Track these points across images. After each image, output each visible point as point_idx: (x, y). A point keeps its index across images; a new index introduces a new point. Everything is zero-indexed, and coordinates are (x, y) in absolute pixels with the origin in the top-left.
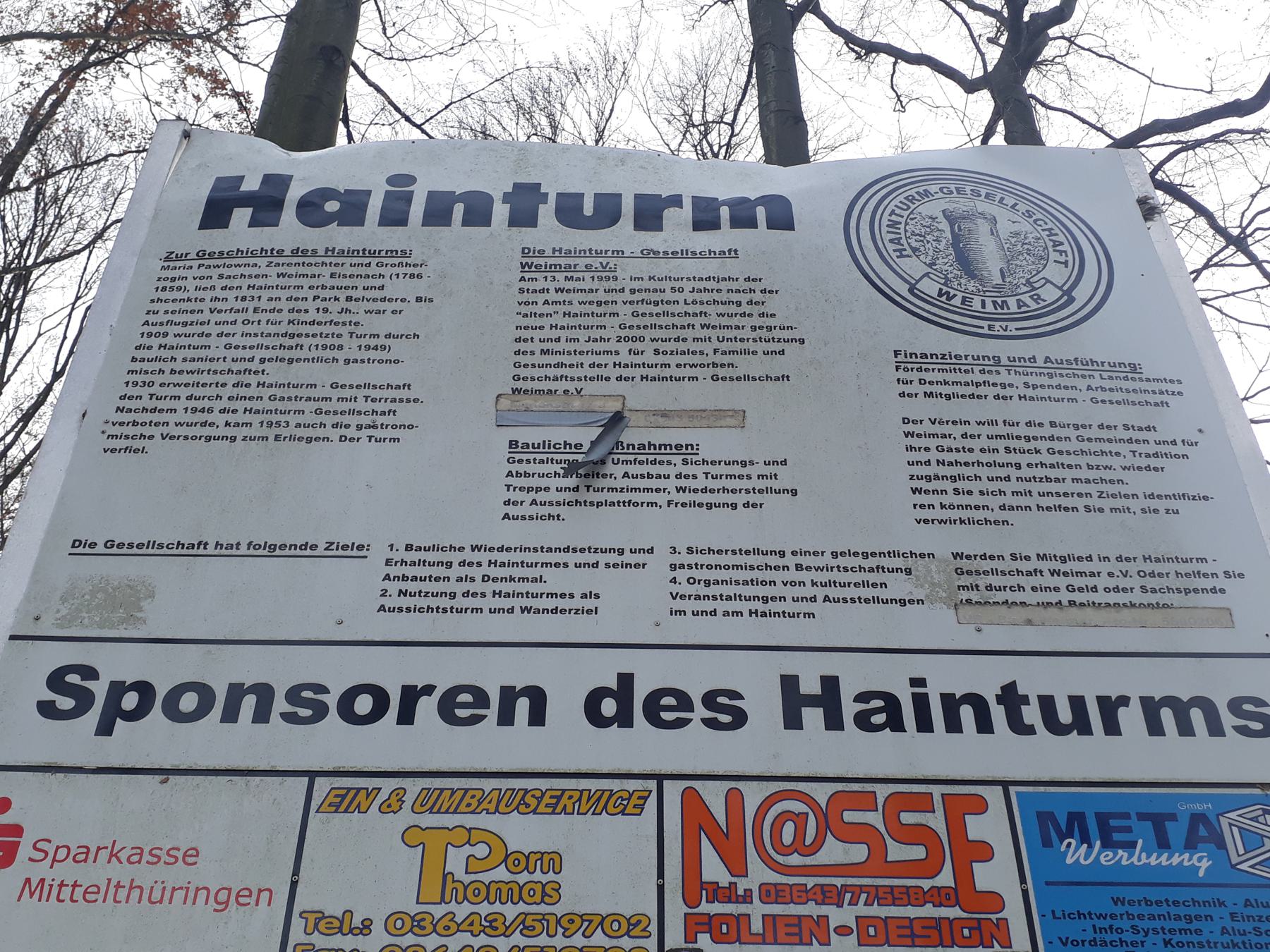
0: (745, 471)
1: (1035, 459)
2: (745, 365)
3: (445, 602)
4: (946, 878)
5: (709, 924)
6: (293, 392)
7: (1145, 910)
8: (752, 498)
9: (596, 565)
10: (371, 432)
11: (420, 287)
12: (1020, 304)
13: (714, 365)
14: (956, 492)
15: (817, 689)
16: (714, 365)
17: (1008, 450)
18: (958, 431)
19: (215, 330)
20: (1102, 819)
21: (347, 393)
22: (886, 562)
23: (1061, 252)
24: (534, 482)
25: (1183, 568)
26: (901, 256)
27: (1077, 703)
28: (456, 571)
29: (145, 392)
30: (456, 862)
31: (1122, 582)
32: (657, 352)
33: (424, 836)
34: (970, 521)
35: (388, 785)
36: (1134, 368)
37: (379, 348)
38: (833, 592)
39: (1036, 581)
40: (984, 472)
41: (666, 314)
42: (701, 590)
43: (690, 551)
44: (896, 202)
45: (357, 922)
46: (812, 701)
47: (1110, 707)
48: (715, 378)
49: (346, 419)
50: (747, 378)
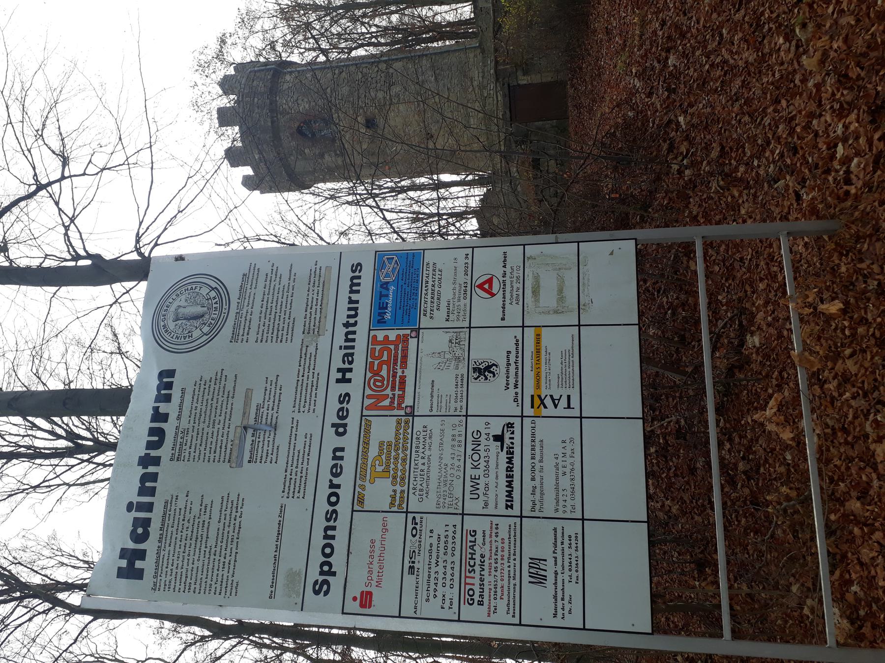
0: (269, 390)
1: (274, 307)
2: (229, 387)
3: (303, 479)
4: (392, 347)
5: (399, 404)
6: (220, 535)
7: (402, 303)
8: (278, 388)
9: (296, 435)
10: (239, 508)
11: (182, 496)
12: (216, 303)
13: (228, 397)
14: (283, 330)
15: (341, 374)
16: (228, 397)
17: (270, 314)
18: (262, 328)
19: (191, 566)
20: (380, 308)
21: (223, 517)
22: (304, 352)
23: (196, 288)
24: (264, 455)
25: (313, 275)
26: (192, 336)
27: (349, 309)
28: (293, 477)
29: (213, 586)
30: (379, 469)
31: (316, 291)
32: (220, 416)
33: (372, 478)
34: (293, 328)
35: (357, 489)
36: (244, 275)
37: (205, 508)
38: (312, 367)
39: (313, 313)
40: (277, 322)
41: (205, 412)
42: (307, 404)
43: (294, 407)
44: (167, 336)
45: (393, 493)
46: (344, 375)
47: (351, 301)
48: (233, 397)
49: (233, 516)
50: (234, 388)
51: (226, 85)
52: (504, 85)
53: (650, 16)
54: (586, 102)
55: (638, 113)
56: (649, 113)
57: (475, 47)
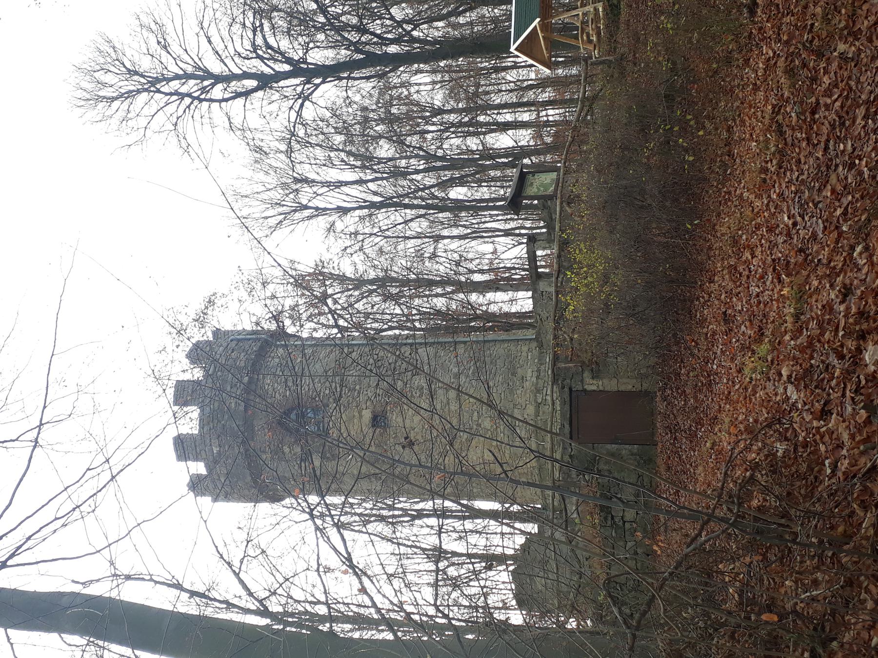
51: (197, 354)
52: (563, 388)
53: (815, 283)
54: (686, 423)
55: (796, 445)
56: (822, 448)
57: (531, 339)
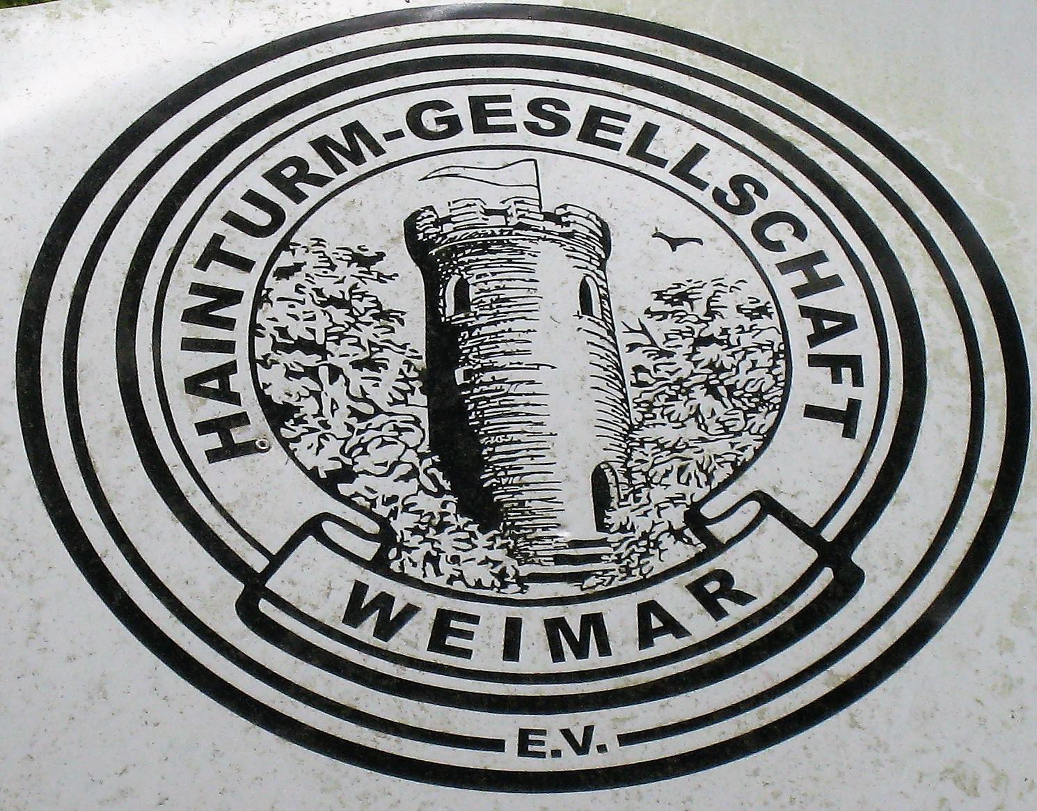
26: (230, 450)
44: (232, 199)
